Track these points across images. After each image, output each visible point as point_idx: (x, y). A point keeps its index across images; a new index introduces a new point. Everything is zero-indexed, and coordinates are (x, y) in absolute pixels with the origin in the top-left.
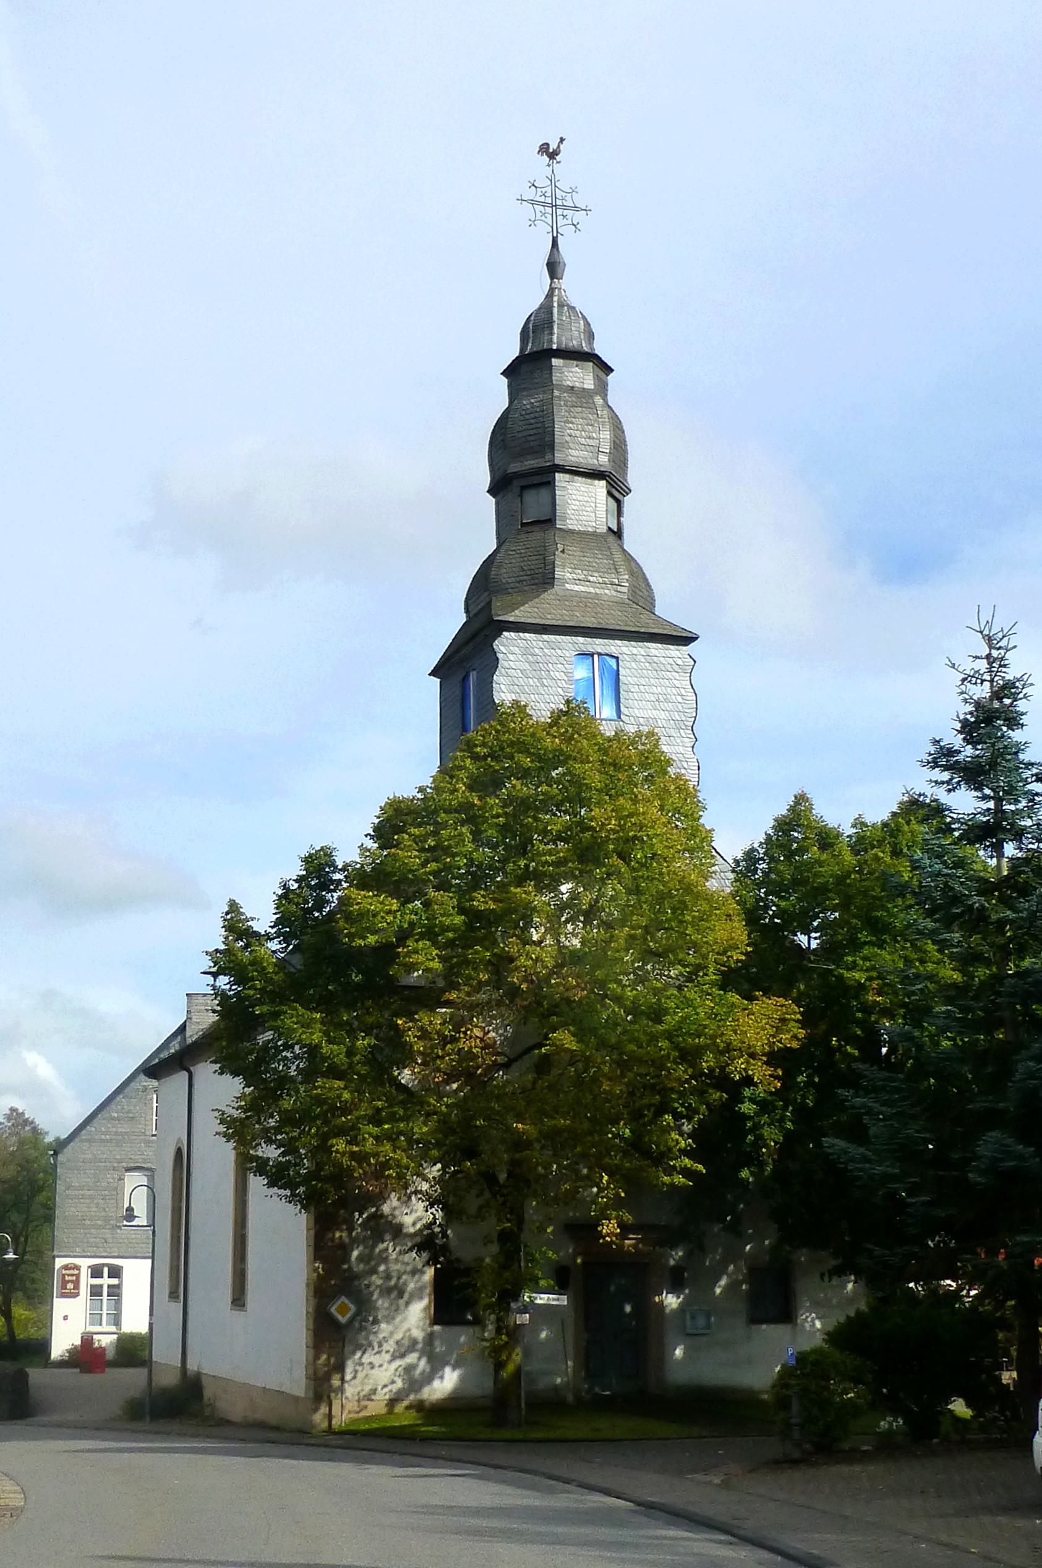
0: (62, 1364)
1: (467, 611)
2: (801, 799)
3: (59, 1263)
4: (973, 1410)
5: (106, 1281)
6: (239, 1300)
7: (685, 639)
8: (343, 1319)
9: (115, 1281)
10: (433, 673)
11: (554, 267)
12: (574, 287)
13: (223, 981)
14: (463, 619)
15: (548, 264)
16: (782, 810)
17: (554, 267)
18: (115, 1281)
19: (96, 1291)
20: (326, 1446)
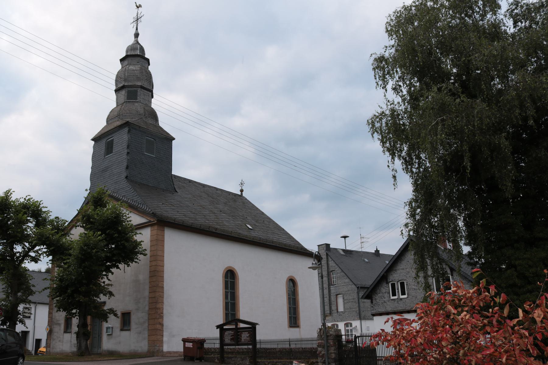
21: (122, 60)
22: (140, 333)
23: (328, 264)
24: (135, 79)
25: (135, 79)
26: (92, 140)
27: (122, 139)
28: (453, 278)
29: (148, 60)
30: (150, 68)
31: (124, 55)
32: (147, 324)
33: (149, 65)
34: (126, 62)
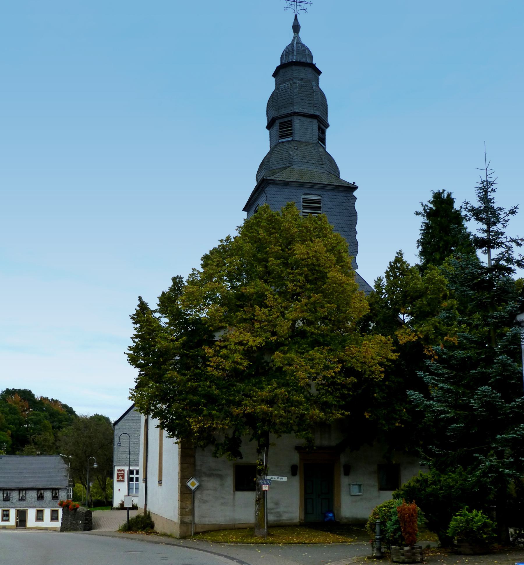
0: (117, 509)
1: (257, 180)
2: (400, 253)
3: (116, 469)
4: (473, 510)
5: (134, 476)
6: (160, 482)
7: (297, 69)
8: (193, 488)
9: (131, 476)
10: (244, 210)
11: (296, 28)
12: (305, 38)
13: (137, 340)
15: (293, 27)
16: (393, 259)
17: (296, 28)
18: (131, 476)
19: (131, 480)
20: (178, 546)
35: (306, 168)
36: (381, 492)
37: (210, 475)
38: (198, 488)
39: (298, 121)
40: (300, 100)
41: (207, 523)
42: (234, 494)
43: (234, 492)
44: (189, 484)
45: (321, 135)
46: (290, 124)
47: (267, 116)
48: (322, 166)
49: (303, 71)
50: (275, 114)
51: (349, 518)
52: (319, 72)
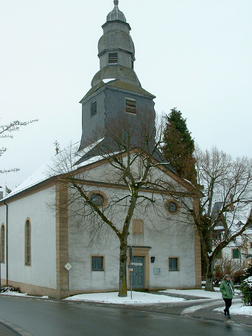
1: (92, 85)
8: (68, 269)
12: (121, 7)
14: (91, 87)
21: (103, 27)
22: (189, 273)
23: (118, 168)
24: (116, 43)
25: (116, 43)
26: (80, 102)
27: (100, 101)
28: (58, 303)
29: (128, 25)
30: (131, 33)
31: (105, 21)
32: (194, 267)
33: (130, 29)
34: (107, 28)
35: (127, 82)
36: (170, 272)
37: (77, 262)
38: (70, 269)
39: (121, 54)
40: (122, 43)
41: (76, 289)
42: (91, 273)
43: (91, 272)
44: (66, 267)
45: (115, 65)
46: (116, 55)
47: (99, 48)
48: (136, 82)
49: (123, 27)
50: (104, 48)
51: (154, 287)
52: (130, 29)
